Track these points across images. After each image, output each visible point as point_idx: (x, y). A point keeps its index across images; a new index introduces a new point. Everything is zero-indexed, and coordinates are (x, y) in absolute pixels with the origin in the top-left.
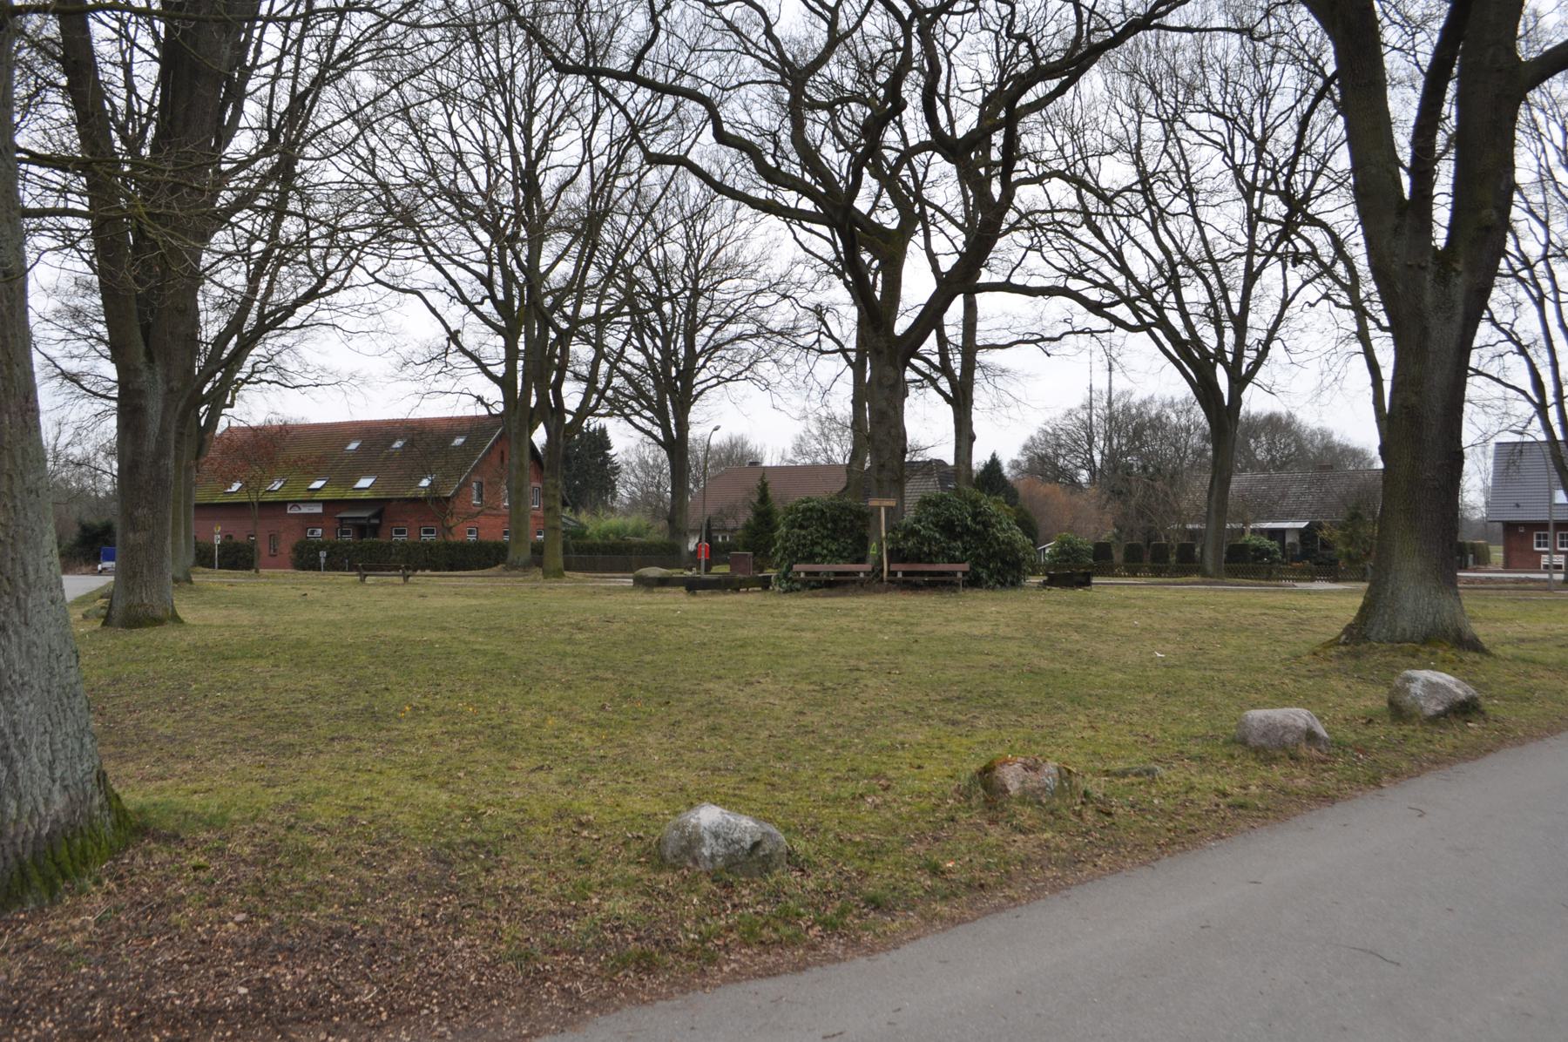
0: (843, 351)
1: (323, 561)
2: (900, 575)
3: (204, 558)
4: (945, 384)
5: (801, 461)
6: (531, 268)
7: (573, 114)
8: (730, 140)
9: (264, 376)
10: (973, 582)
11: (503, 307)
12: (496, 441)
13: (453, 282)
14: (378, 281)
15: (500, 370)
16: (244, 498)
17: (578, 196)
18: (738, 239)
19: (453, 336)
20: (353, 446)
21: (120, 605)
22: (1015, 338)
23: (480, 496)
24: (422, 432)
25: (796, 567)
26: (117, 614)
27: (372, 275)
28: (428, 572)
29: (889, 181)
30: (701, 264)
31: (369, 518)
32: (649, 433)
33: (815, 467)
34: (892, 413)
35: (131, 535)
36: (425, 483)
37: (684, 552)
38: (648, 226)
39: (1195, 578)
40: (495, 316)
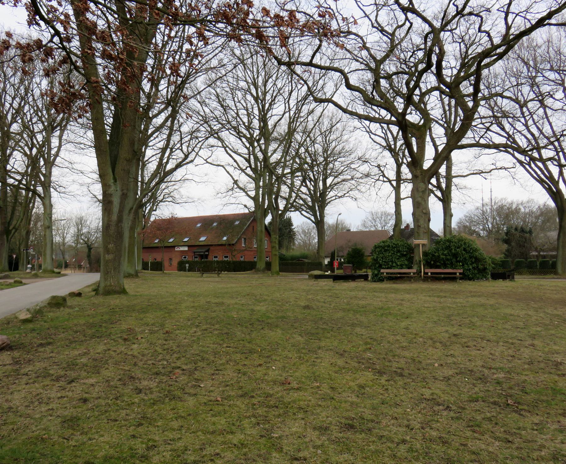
0: (390, 181)
1: (187, 268)
2: (429, 274)
3: (145, 266)
4: (439, 194)
5: (364, 229)
6: (265, 152)
7: (281, 94)
8: (353, 88)
9: (167, 199)
10: (465, 277)
11: (254, 170)
12: (251, 222)
13: (235, 161)
14: (207, 162)
15: (253, 194)
16: (160, 245)
17: (283, 128)
18: (343, 142)
19: (236, 182)
20: (199, 225)
21: (102, 285)
22: (469, 173)
23: (245, 243)
24: (224, 220)
25: (382, 271)
26: (101, 290)
27: (206, 160)
28: (226, 272)
29: (417, 108)
30: (329, 153)
31: (204, 252)
32: (309, 218)
33: (370, 232)
34: (423, 203)
35: (107, 256)
36: (225, 238)
37: (324, 265)
38: (308, 139)
39: (552, 276)
40: (251, 173)
